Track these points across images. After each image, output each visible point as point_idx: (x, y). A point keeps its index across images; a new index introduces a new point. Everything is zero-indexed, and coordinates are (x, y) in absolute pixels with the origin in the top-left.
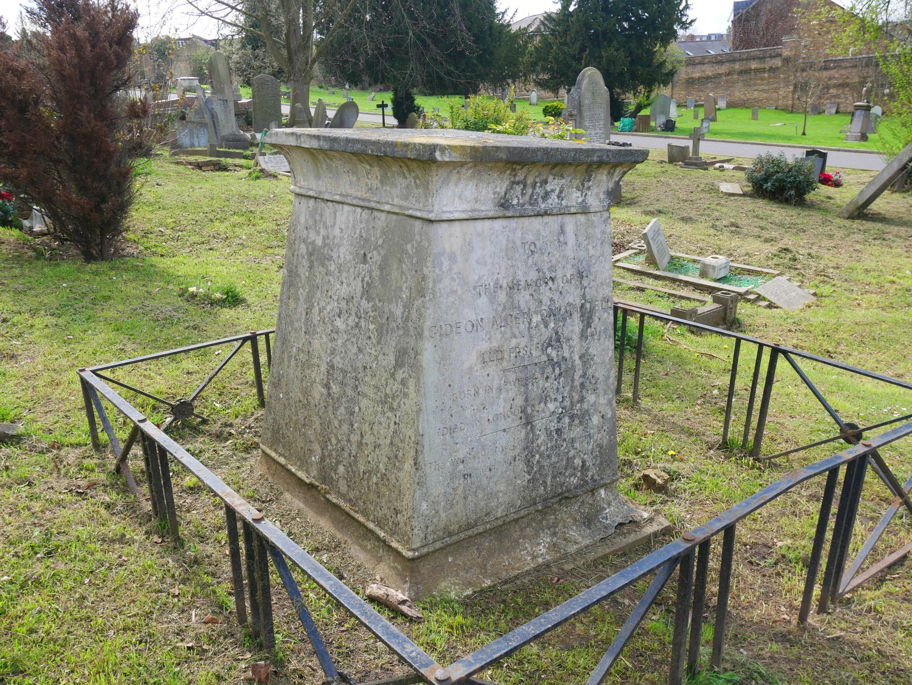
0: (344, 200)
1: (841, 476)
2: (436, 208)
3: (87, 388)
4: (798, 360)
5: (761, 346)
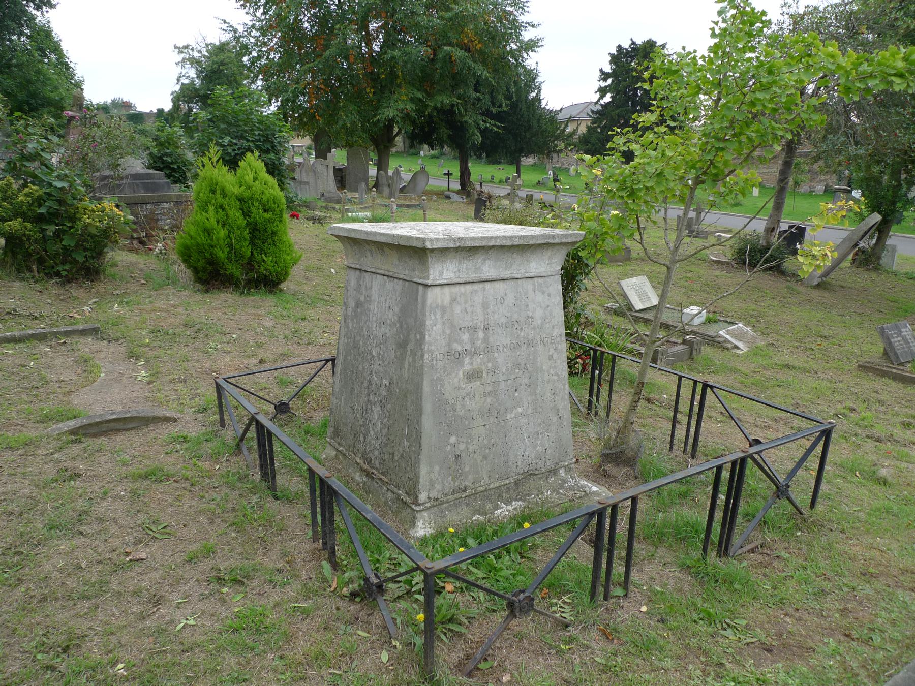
0: (378, 271)
1: (725, 475)
2: (431, 277)
3: (218, 386)
4: (715, 390)
5: (696, 382)
